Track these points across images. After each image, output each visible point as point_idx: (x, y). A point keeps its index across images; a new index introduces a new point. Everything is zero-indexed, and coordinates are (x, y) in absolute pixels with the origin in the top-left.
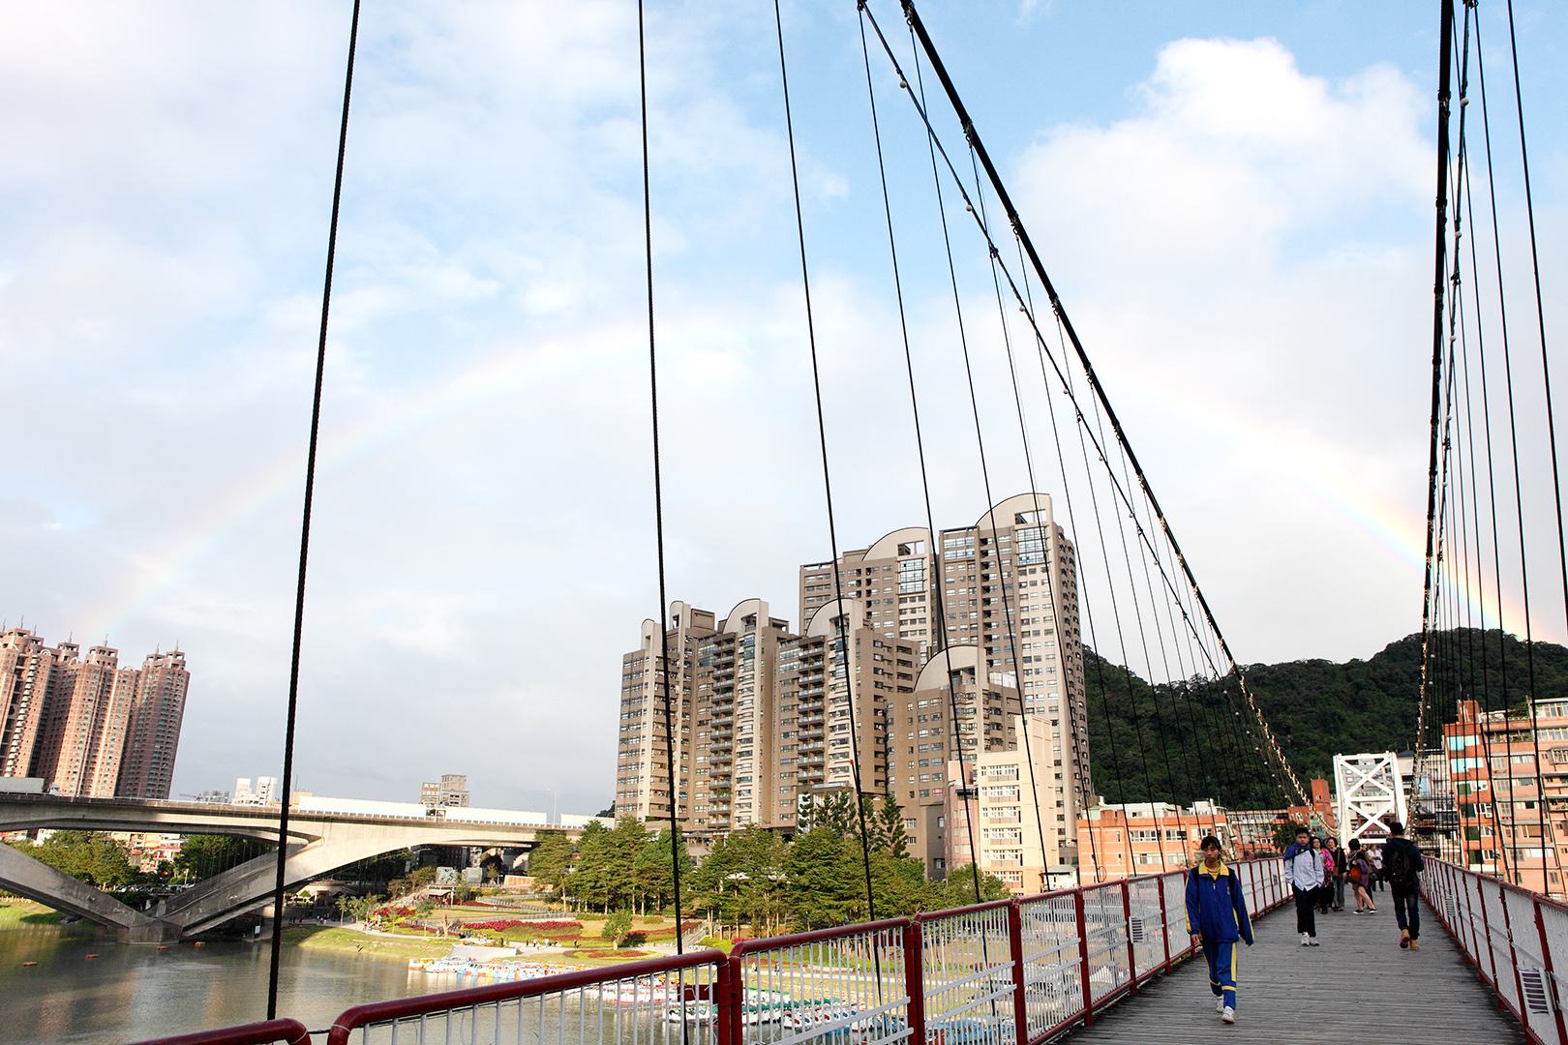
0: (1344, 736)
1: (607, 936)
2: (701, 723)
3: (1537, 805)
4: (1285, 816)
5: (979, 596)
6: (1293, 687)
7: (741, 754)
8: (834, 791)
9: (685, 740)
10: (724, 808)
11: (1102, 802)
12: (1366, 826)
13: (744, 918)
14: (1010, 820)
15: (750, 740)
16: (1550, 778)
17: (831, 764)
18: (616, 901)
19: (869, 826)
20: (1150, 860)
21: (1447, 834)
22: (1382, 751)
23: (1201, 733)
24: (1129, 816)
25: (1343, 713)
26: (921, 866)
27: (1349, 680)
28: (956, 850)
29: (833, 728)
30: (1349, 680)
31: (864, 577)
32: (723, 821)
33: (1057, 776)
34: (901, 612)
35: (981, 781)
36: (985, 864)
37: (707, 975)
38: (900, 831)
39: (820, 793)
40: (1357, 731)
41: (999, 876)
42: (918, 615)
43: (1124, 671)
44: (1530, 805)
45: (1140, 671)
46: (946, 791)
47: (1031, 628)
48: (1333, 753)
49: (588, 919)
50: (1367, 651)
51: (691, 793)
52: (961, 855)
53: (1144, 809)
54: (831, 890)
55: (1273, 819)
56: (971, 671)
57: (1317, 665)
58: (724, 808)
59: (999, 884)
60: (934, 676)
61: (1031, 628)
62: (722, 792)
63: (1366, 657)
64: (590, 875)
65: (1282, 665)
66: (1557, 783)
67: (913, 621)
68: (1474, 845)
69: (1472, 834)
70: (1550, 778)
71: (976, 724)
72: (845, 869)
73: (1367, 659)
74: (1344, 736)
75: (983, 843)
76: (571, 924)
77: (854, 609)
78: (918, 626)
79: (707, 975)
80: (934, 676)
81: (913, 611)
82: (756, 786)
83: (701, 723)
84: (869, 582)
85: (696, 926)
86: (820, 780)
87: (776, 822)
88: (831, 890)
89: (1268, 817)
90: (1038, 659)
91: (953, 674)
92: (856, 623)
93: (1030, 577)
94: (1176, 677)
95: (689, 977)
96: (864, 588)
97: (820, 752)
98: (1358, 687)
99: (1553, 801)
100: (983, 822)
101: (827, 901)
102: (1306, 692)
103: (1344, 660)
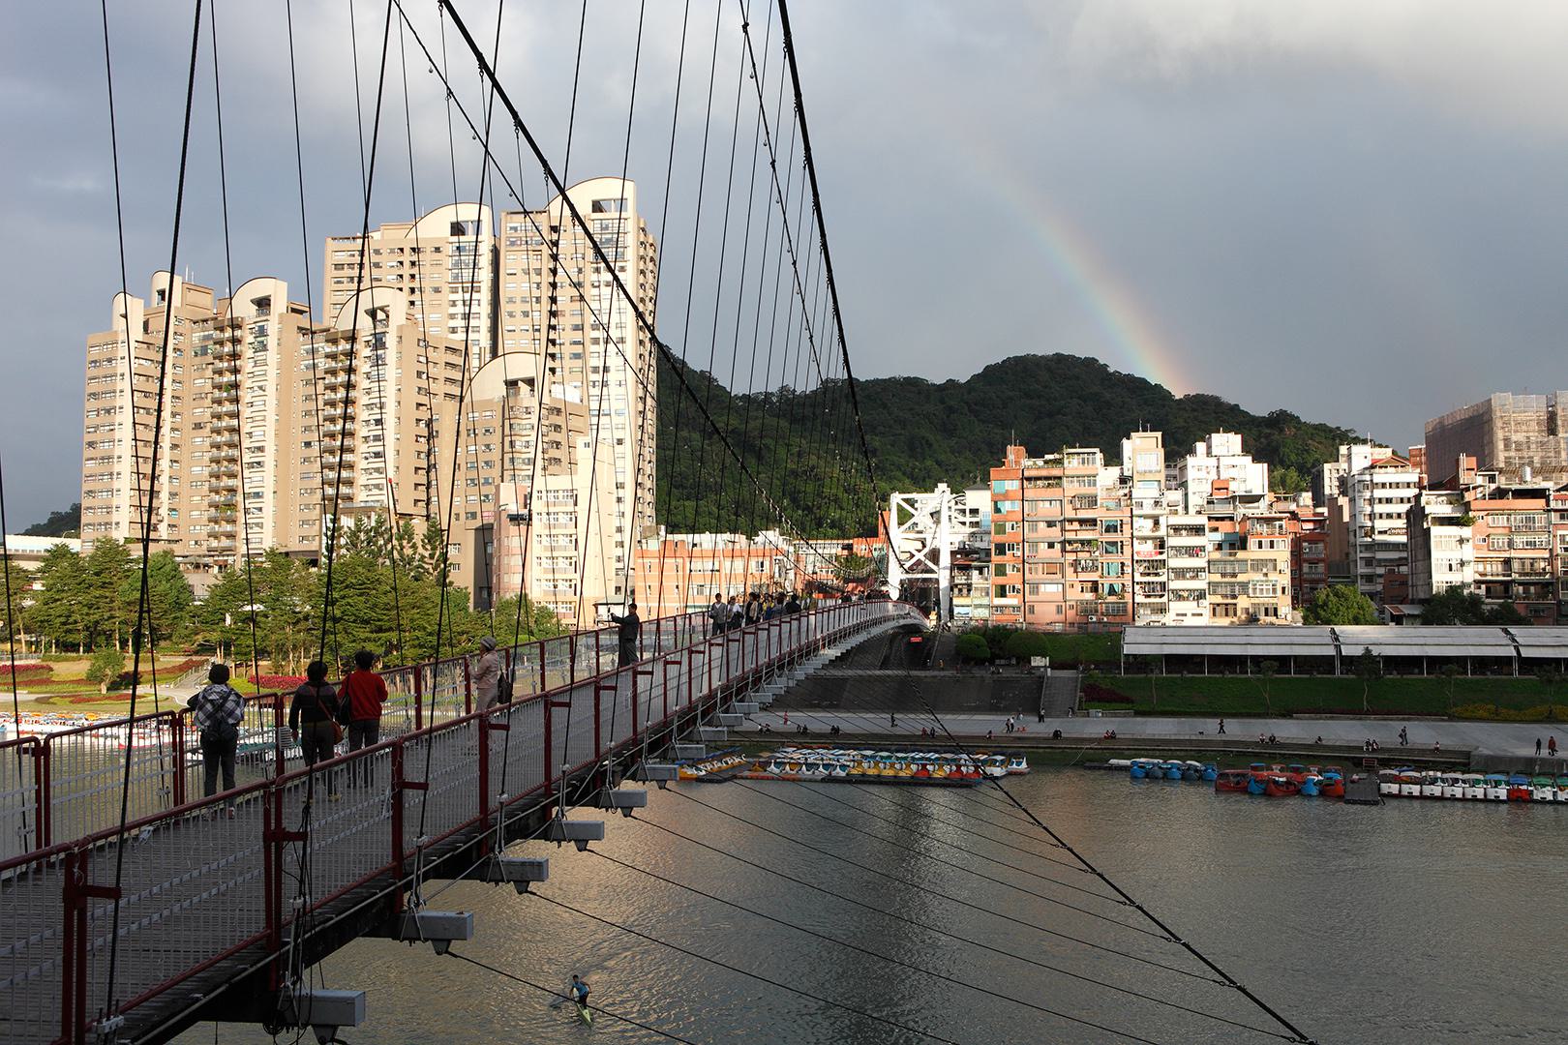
0: (929, 463)
1: (93, 678)
2: (198, 426)
3: (1058, 546)
4: (849, 547)
5: (546, 292)
6: (885, 406)
7: (251, 465)
8: (367, 511)
9: (175, 446)
10: (229, 528)
13: (261, 653)
14: (565, 548)
15: (261, 449)
16: (1071, 521)
18: (94, 638)
19: (408, 551)
23: (782, 452)
25: (931, 438)
26: (466, 596)
27: (942, 402)
28: (505, 578)
31: (407, 257)
32: (225, 542)
33: (619, 500)
34: (454, 304)
35: (537, 506)
36: (537, 594)
37: (271, 701)
38: (445, 557)
39: (349, 512)
40: (942, 457)
41: (551, 607)
43: (706, 378)
44: (1051, 545)
45: (724, 381)
46: (498, 514)
48: (894, 490)
49: (57, 660)
50: (963, 373)
51: (183, 510)
52: (510, 584)
53: (706, 539)
54: (367, 622)
55: (839, 551)
56: (530, 382)
57: (913, 384)
58: (229, 528)
59: (551, 615)
60: (488, 385)
62: (225, 510)
63: (963, 378)
64: (59, 609)
65: (877, 382)
66: (1076, 526)
68: (1001, 580)
69: (1000, 570)
70: (1071, 521)
71: (527, 437)
72: (385, 599)
73: (963, 381)
75: (535, 572)
76: (35, 667)
77: (396, 302)
79: (271, 701)
80: (488, 385)
82: (268, 502)
83: (198, 426)
85: (202, 663)
87: (294, 546)
88: (367, 622)
89: (834, 548)
91: (512, 384)
92: (398, 317)
94: (758, 388)
95: (264, 701)
96: (407, 271)
98: (951, 410)
99: (1070, 542)
100: (536, 549)
101: (363, 633)
103: (940, 380)
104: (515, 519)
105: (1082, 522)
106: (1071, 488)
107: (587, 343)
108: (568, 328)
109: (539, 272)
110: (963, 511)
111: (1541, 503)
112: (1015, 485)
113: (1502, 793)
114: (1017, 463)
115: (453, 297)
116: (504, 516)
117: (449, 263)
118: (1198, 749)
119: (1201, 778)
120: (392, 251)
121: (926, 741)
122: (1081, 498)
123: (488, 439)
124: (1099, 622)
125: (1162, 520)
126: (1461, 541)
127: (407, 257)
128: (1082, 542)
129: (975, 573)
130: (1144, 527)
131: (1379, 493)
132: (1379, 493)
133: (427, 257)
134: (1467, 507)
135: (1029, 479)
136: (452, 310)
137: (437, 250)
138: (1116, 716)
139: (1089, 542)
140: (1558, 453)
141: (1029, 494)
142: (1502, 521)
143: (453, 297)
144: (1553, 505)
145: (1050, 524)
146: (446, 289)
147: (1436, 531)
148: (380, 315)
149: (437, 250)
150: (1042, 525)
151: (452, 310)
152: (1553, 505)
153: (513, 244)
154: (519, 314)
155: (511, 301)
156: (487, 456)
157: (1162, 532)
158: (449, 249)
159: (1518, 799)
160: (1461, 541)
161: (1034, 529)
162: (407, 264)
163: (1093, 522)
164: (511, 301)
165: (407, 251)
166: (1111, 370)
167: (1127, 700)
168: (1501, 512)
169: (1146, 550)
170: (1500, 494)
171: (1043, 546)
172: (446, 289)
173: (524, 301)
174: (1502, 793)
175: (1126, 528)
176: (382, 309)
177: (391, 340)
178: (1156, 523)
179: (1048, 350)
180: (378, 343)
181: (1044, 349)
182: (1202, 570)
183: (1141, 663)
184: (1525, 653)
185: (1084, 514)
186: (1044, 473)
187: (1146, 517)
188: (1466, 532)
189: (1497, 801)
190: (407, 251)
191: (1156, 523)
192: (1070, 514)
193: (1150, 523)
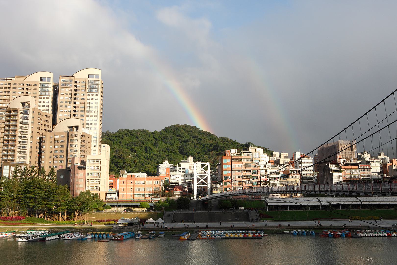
3: (241, 177)
6: (137, 138)
8: (20, 165)
11: (126, 173)
12: (200, 181)
16: (244, 170)
17: (17, 155)
20: (140, 190)
21: (220, 184)
22: (206, 162)
24: (136, 177)
29: (19, 142)
30: (154, 137)
31: (25, 87)
34: (40, 102)
39: (13, 165)
42: (46, 104)
44: (239, 177)
47: (90, 114)
57: (144, 131)
61: (90, 114)
66: (245, 172)
67: (44, 106)
69: (225, 184)
70: (244, 170)
74: (152, 154)
78: (45, 108)
81: (44, 102)
84: (27, 89)
86: (13, 161)
90: (91, 124)
91: (70, 127)
93: (91, 97)
96: (73, 101)
97: (14, 151)
98: (156, 139)
99: (244, 176)
102: (141, 140)
103: (153, 131)
104: (80, 168)
105: (247, 171)
106: (244, 162)
107: (85, 116)
108: (79, 111)
109: (71, 94)
110: (180, 168)
111: (356, 167)
112: (229, 161)
113: (386, 234)
114: (229, 155)
115: (40, 100)
116: (76, 167)
117: (39, 89)
118: (310, 228)
119: (311, 235)
120: (20, 84)
121: (248, 229)
122: (248, 164)
123: (62, 144)
124: (252, 198)
125: (268, 170)
126: (340, 176)
127: (25, 87)
128: (247, 176)
129: (218, 185)
130: (263, 172)
131: (303, 165)
132: (303, 165)
133: (32, 87)
134: (340, 168)
135: (233, 159)
136: (39, 104)
137: (35, 85)
138: (270, 221)
139: (249, 176)
140: (353, 155)
141: (233, 163)
142: (348, 171)
143: (40, 100)
144: (360, 167)
145: (239, 171)
146: (38, 97)
147: (334, 174)
148: (26, 104)
149: (35, 85)
150: (237, 172)
151: (39, 104)
152: (360, 167)
153: (63, 85)
154: (64, 107)
155: (62, 102)
156: (62, 149)
157: (268, 173)
158: (39, 85)
159: (389, 236)
160: (340, 176)
161: (235, 173)
162: (25, 89)
163: (250, 171)
164: (62, 102)
165: (25, 85)
166: (200, 130)
167: (272, 217)
168: (348, 169)
169: (264, 178)
170: (347, 165)
171: (237, 177)
172: (38, 97)
173: (66, 102)
174: (386, 234)
175: (259, 173)
176: (27, 102)
177: (30, 112)
178: (266, 171)
179: (192, 125)
180: (26, 113)
181: (182, 123)
182: (278, 184)
183: (271, 208)
184: (364, 203)
185: (247, 169)
186: (237, 158)
187: (264, 170)
188: (341, 174)
189: (385, 236)
190: (25, 85)
191: (266, 171)
192: (244, 168)
193: (264, 171)
